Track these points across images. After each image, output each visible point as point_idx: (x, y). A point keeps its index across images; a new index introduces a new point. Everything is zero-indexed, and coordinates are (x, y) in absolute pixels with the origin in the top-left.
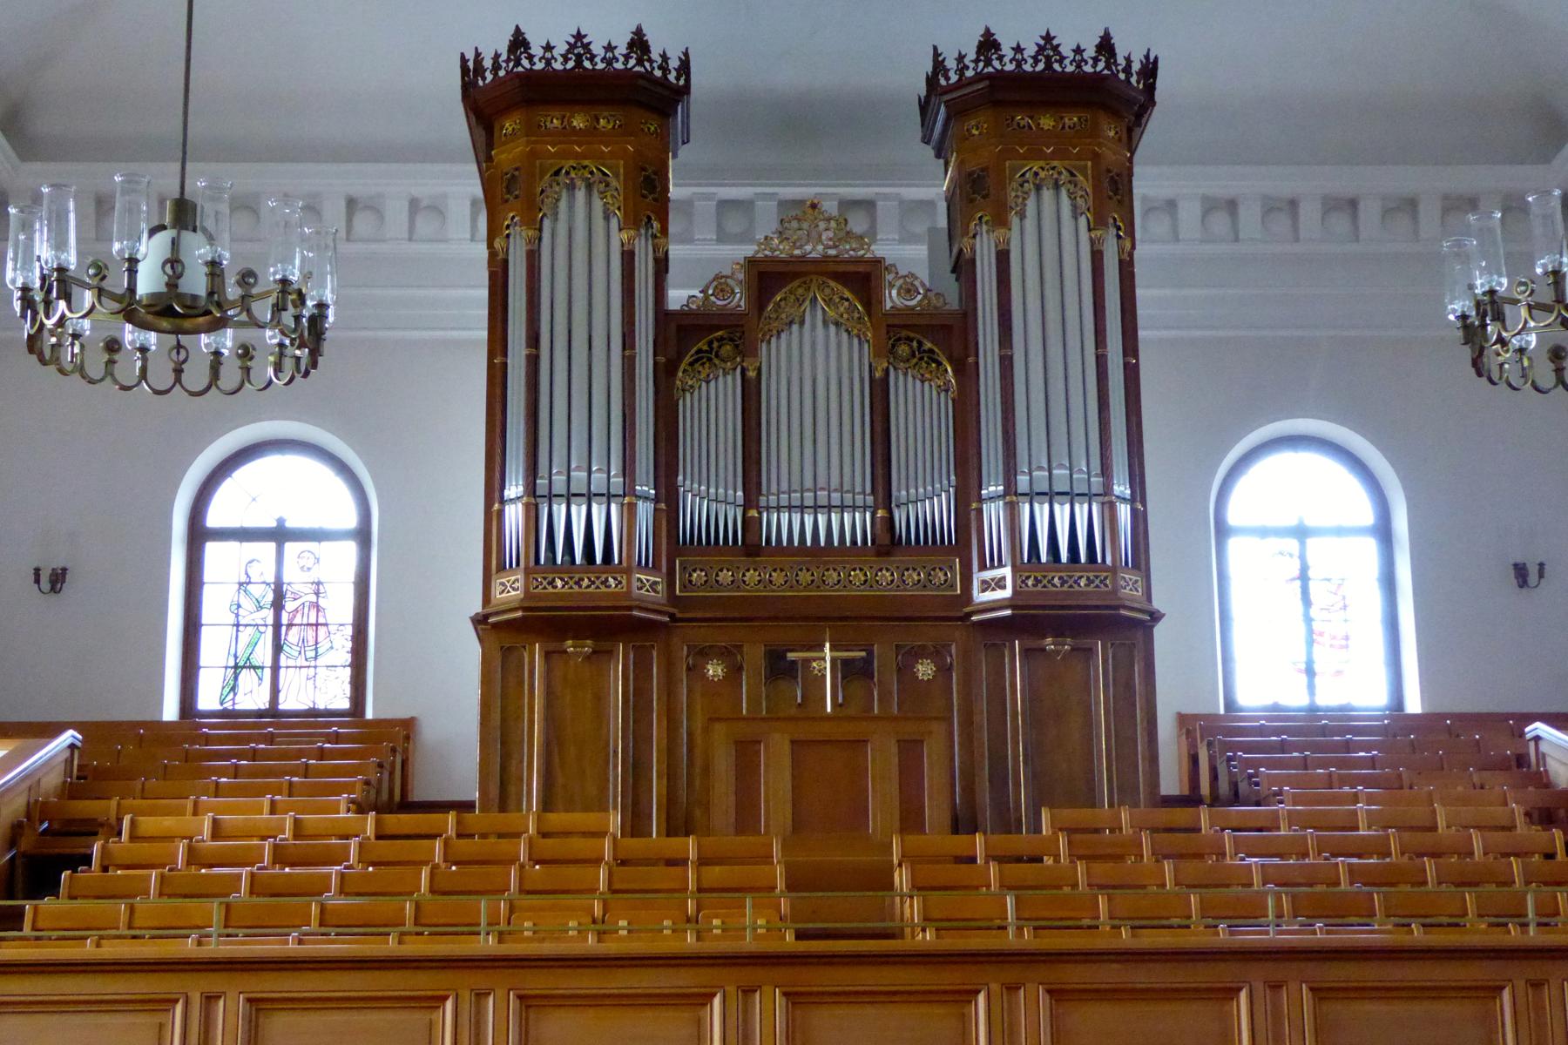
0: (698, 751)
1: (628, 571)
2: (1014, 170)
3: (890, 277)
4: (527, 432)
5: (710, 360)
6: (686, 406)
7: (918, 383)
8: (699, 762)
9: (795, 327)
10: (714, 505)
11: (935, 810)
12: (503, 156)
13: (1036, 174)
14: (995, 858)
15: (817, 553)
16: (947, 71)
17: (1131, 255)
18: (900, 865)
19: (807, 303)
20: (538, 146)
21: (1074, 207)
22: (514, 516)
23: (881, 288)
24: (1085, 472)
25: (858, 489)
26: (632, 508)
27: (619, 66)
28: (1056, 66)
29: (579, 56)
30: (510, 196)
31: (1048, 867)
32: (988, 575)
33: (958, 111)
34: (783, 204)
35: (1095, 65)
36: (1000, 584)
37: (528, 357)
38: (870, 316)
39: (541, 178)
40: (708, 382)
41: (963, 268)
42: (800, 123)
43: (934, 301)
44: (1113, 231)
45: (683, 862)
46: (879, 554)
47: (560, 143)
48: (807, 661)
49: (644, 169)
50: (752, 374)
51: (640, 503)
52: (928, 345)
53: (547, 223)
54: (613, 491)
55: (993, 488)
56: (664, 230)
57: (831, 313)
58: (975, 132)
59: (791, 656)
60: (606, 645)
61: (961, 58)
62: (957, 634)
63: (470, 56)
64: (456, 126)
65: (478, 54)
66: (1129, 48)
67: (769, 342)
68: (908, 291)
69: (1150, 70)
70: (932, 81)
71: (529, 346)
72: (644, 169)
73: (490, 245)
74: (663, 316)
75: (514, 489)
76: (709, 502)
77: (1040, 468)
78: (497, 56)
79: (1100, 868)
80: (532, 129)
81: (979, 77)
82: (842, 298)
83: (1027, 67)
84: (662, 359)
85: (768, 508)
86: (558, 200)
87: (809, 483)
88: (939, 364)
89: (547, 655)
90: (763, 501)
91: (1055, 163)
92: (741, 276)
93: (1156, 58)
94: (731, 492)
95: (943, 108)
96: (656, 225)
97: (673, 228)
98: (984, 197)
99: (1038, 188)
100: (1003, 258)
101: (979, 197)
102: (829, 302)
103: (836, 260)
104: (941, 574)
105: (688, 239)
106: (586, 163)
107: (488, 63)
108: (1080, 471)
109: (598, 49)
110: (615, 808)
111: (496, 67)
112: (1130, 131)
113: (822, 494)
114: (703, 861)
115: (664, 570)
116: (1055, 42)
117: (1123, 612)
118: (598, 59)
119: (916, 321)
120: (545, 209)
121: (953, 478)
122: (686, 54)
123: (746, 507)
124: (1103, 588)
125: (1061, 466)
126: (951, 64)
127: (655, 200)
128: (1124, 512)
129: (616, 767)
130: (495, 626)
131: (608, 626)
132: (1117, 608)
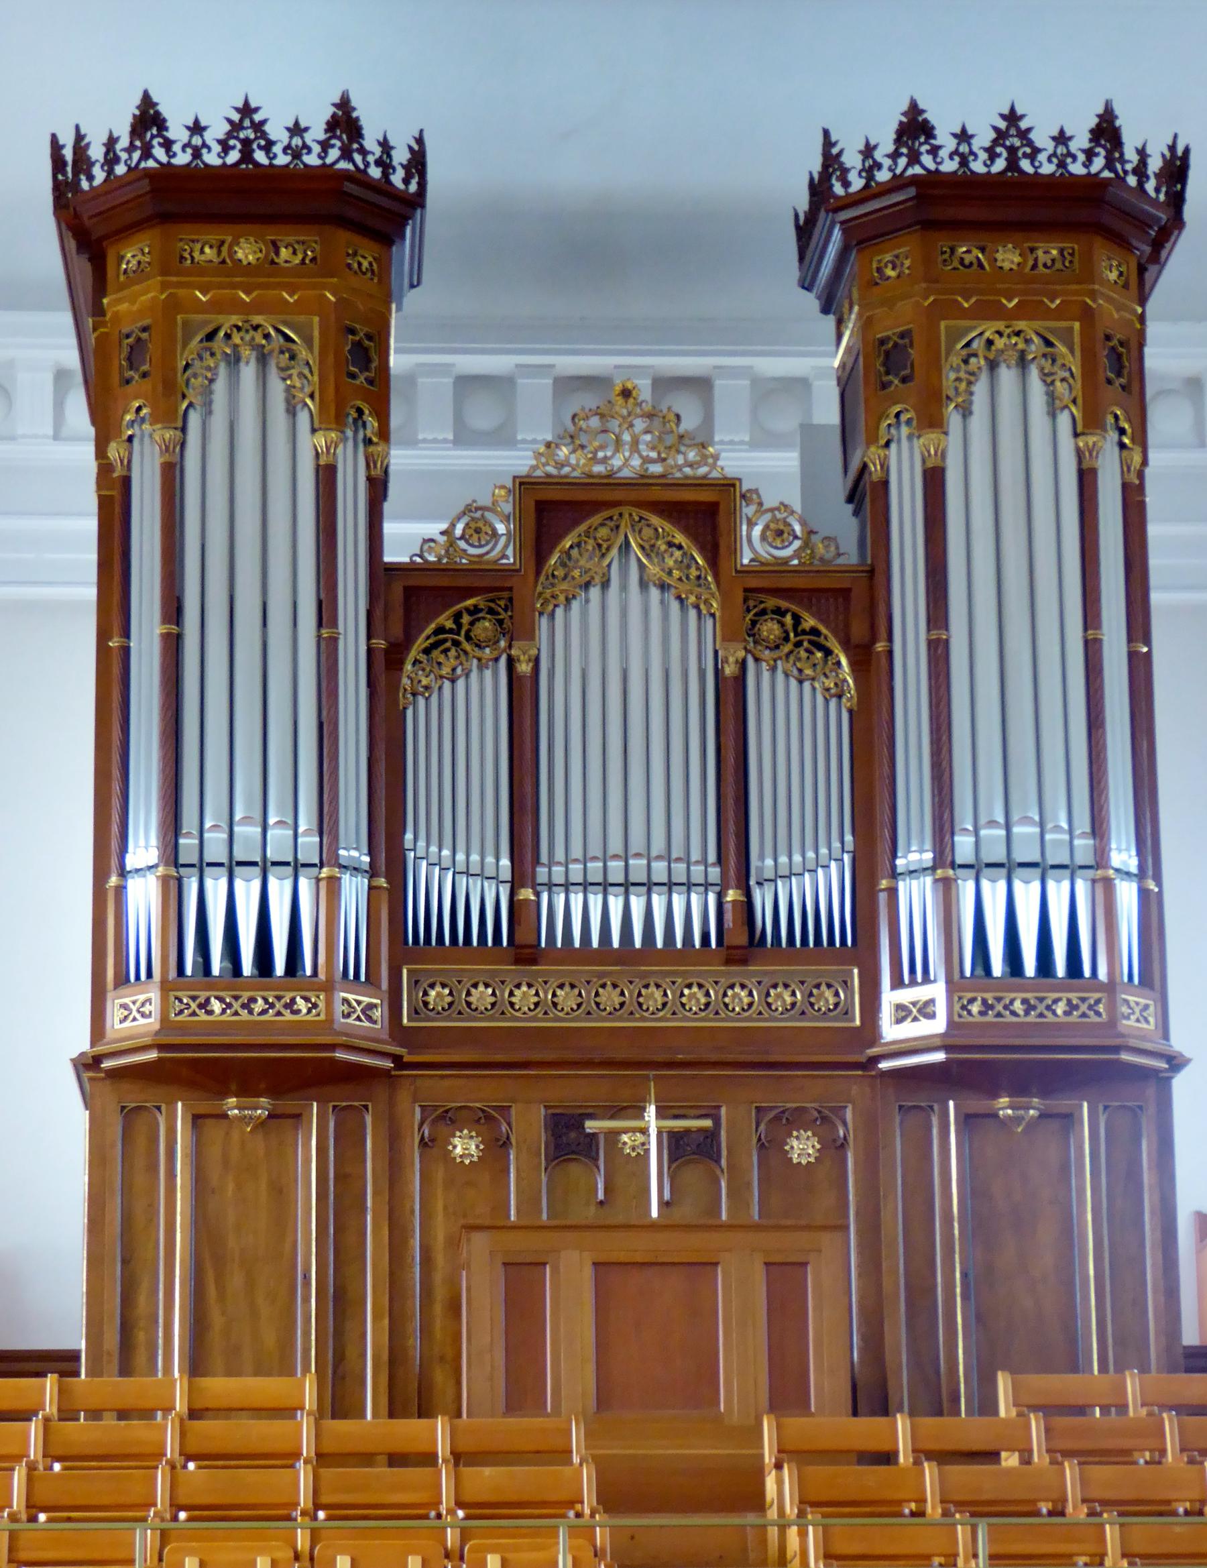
0: (438, 1277)
1: (328, 988)
2: (954, 337)
3: (749, 510)
4: (164, 758)
5: (456, 643)
6: (419, 720)
7: (793, 683)
8: (440, 1294)
9: (595, 592)
10: (462, 881)
11: (825, 1378)
12: (123, 307)
13: (990, 343)
14: (931, 1455)
15: (629, 958)
16: (845, 171)
17: (1141, 475)
18: (778, 1466)
19: (614, 552)
20: (181, 292)
21: (1051, 397)
22: (143, 897)
23: (734, 530)
24: (1065, 833)
25: (695, 855)
26: (334, 884)
27: (312, 160)
28: (1025, 165)
29: (246, 143)
30: (127, 374)
31: (1009, 1471)
32: (906, 996)
33: (862, 238)
34: (567, 385)
35: (1088, 162)
36: (925, 1010)
37: (166, 637)
38: (716, 576)
39: (185, 346)
40: (453, 681)
41: (867, 495)
42: (595, 250)
43: (820, 549)
44: (1113, 436)
45: (429, 1459)
46: (729, 962)
47: (221, 286)
48: (614, 1134)
49: (353, 331)
50: (524, 668)
51: (346, 878)
52: (810, 622)
53: (194, 419)
54: (302, 858)
55: (915, 854)
56: (384, 434)
57: (653, 569)
58: (890, 272)
59: (591, 1126)
60: (289, 1105)
61: (868, 150)
62: (855, 1090)
63: (67, 140)
64: (42, 249)
65: (79, 137)
66: (1145, 134)
67: (552, 616)
68: (780, 533)
69: (1177, 169)
70: (819, 190)
71: (166, 619)
72: (353, 331)
73: (101, 453)
74: (381, 575)
75: (143, 849)
76: (456, 875)
77: (992, 823)
78: (111, 142)
79: (1101, 1472)
80: (170, 265)
81: (898, 183)
82: (670, 544)
83: (978, 167)
84: (380, 643)
85: (550, 886)
86: (211, 381)
87: (615, 846)
88: (828, 652)
89: (197, 1120)
90: (542, 873)
91: (1021, 325)
92: (507, 508)
93: (1187, 151)
94: (490, 859)
95: (837, 234)
96: (372, 422)
97: (395, 421)
98: (904, 380)
99: (993, 365)
100: (934, 480)
101: (893, 378)
102: (649, 550)
103: (663, 482)
104: (829, 994)
105: (412, 443)
106: (257, 319)
107: (96, 152)
108: (1057, 828)
109: (277, 131)
110: (306, 1369)
111: (111, 160)
112: (1142, 270)
113: (637, 863)
114: (458, 1458)
115: (385, 985)
116: (1023, 125)
117: (1125, 1057)
118: (277, 149)
119: (786, 583)
120: (192, 396)
121: (849, 838)
122: (420, 140)
123: (515, 884)
124: (1094, 1019)
125: (1026, 820)
126: (852, 160)
127: (370, 382)
128: (1127, 895)
129: (307, 1300)
130: (114, 1074)
131: (294, 1075)
132: (1116, 1049)
